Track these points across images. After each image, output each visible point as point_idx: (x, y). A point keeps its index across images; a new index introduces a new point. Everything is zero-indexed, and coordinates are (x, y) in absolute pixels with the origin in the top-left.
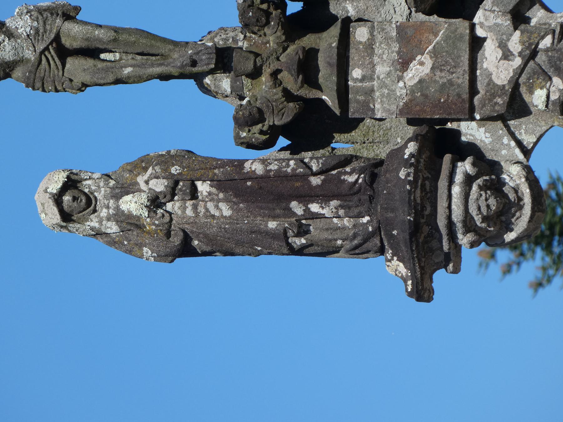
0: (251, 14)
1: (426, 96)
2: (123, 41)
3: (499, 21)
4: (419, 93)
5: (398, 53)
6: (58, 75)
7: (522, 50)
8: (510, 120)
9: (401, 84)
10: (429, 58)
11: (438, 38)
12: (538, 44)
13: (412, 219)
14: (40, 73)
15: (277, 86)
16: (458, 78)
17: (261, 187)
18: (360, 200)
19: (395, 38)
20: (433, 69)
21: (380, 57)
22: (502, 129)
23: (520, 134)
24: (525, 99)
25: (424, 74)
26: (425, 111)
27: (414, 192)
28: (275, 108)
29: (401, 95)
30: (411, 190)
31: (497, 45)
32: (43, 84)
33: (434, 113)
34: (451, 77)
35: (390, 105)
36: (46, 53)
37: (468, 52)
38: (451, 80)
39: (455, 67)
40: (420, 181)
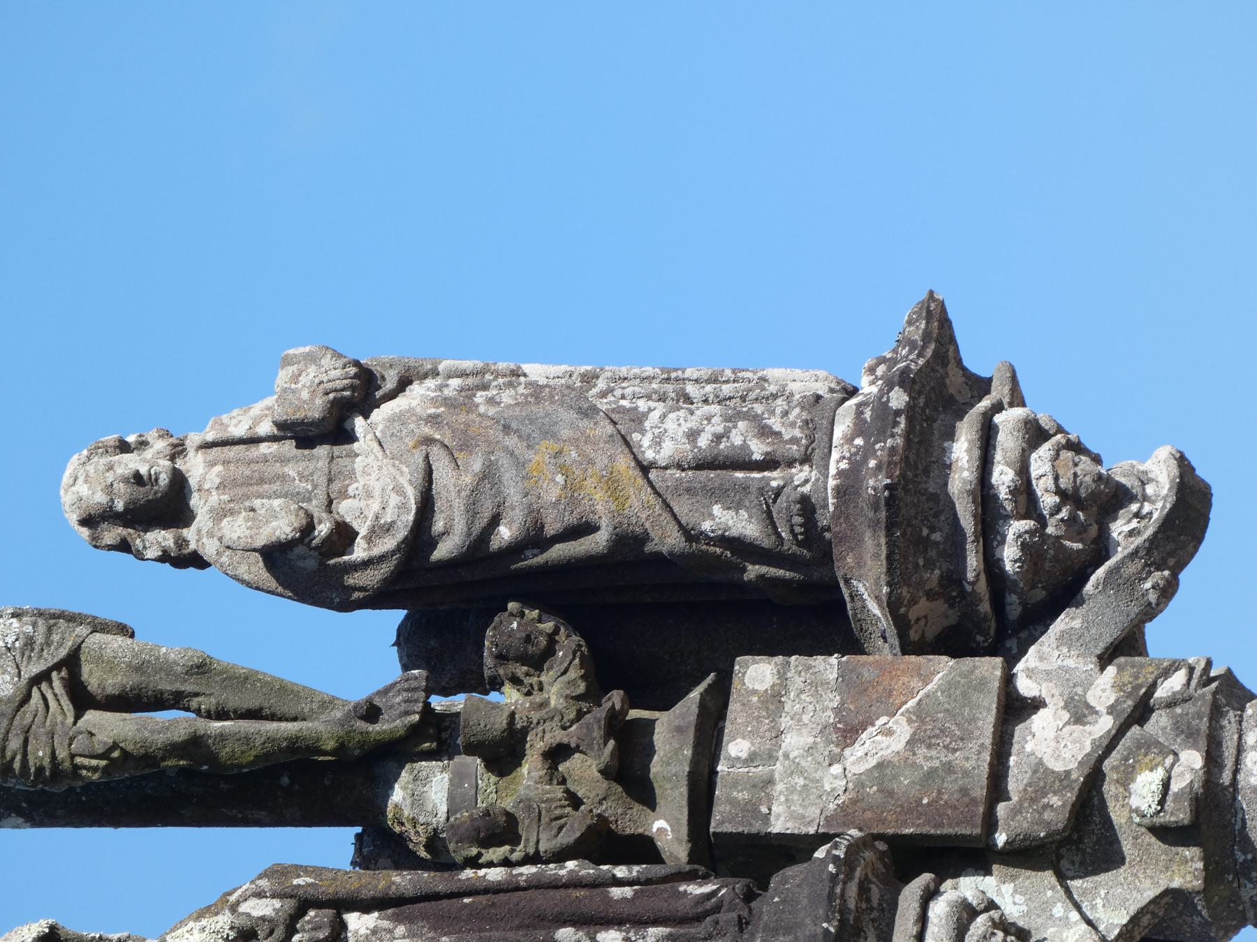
0: (515, 625)
1: (891, 794)
2: (221, 673)
3: (1071, 663)
4: (875, 788)
5: (837, 711)
6: (62, 723)
7: (1116, 701)
8: (1072, 879)
9: (836, 769)
10: (905, 723)
11: (929, 687)
12: (1153, 687)
13: (832, 930)
14: (22, 719)
15: (555, 782)
16: (967, 759)
17: (493, 904)
18: (717, 923)
19: (833, 683)
20: (912, 743)
21: (797, 718)
22: (1052, 888)
23: (1094, 907)
24: (1113, 817)
25: (889, 751)
26: (883, 821)
27: (845, 883)
28: (544, 812)
29: (833, 790)
30: (837, 874)
31: (1062, 704)
32: (26, 741)
33: (905, 824)
34: (951, 757)
35: (805, 807)
36: (44, 686)
37: (994, 711)
38: (950, 762)
39: (962, 739)
40: (859, 869)
